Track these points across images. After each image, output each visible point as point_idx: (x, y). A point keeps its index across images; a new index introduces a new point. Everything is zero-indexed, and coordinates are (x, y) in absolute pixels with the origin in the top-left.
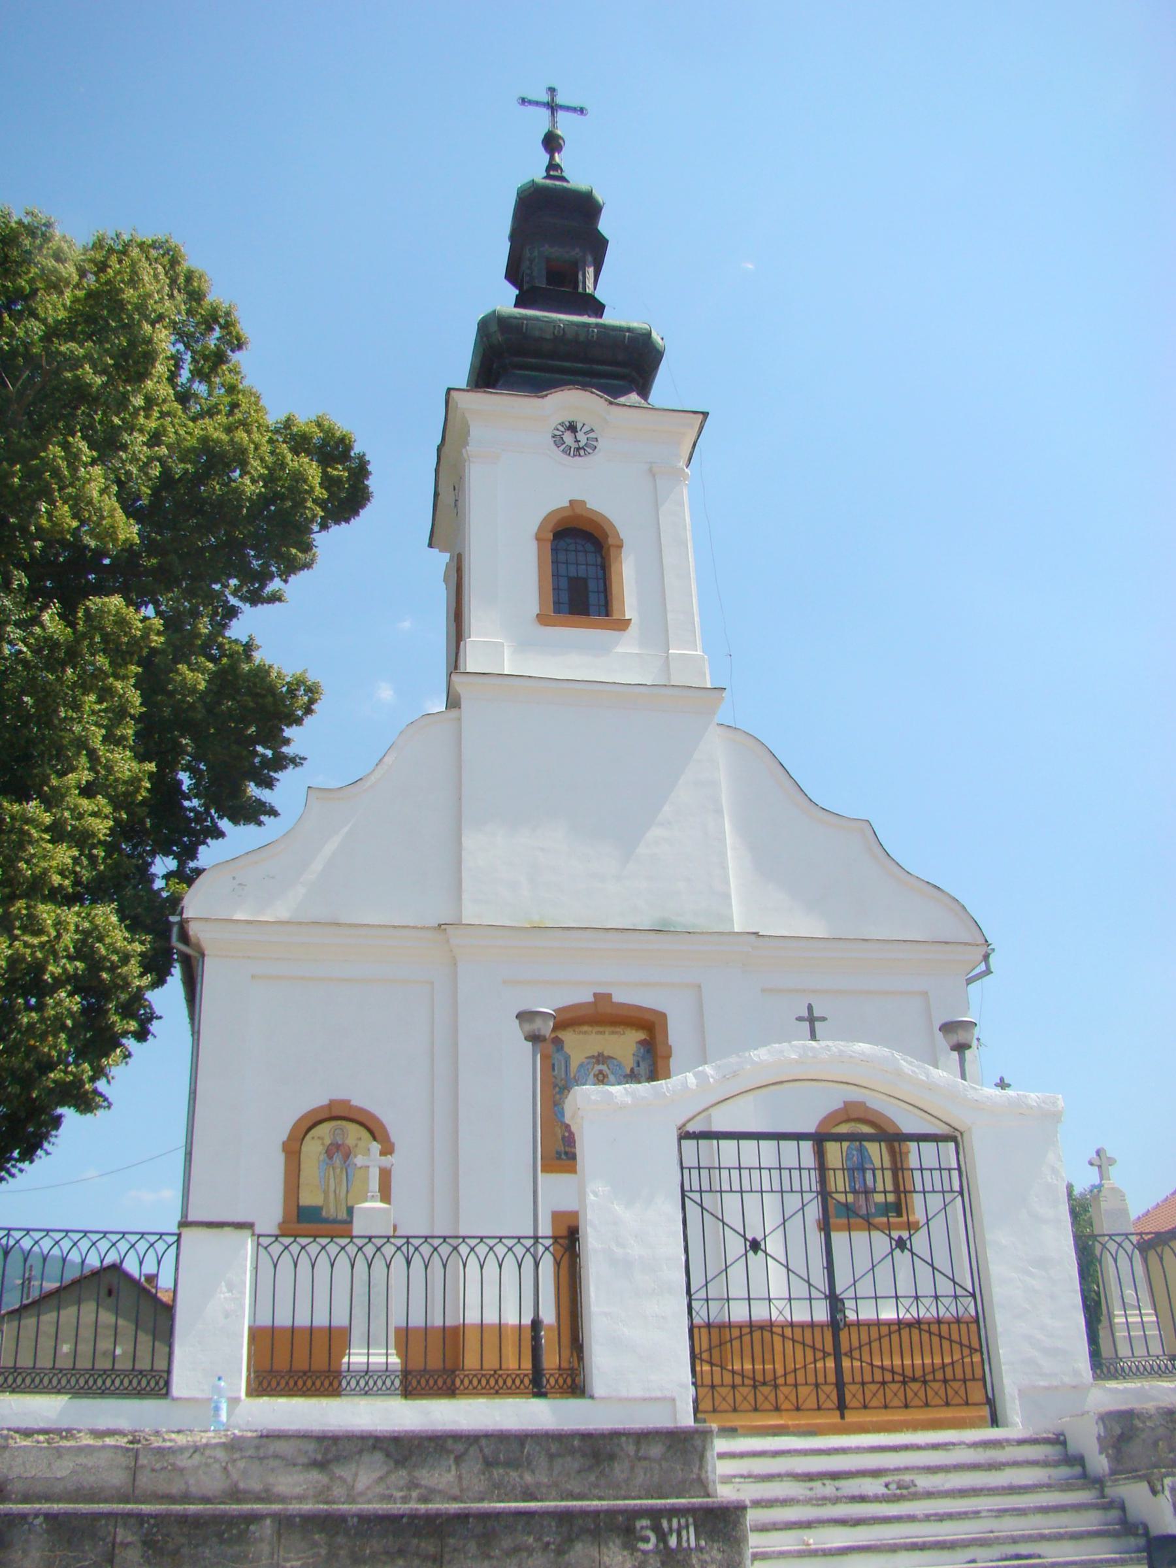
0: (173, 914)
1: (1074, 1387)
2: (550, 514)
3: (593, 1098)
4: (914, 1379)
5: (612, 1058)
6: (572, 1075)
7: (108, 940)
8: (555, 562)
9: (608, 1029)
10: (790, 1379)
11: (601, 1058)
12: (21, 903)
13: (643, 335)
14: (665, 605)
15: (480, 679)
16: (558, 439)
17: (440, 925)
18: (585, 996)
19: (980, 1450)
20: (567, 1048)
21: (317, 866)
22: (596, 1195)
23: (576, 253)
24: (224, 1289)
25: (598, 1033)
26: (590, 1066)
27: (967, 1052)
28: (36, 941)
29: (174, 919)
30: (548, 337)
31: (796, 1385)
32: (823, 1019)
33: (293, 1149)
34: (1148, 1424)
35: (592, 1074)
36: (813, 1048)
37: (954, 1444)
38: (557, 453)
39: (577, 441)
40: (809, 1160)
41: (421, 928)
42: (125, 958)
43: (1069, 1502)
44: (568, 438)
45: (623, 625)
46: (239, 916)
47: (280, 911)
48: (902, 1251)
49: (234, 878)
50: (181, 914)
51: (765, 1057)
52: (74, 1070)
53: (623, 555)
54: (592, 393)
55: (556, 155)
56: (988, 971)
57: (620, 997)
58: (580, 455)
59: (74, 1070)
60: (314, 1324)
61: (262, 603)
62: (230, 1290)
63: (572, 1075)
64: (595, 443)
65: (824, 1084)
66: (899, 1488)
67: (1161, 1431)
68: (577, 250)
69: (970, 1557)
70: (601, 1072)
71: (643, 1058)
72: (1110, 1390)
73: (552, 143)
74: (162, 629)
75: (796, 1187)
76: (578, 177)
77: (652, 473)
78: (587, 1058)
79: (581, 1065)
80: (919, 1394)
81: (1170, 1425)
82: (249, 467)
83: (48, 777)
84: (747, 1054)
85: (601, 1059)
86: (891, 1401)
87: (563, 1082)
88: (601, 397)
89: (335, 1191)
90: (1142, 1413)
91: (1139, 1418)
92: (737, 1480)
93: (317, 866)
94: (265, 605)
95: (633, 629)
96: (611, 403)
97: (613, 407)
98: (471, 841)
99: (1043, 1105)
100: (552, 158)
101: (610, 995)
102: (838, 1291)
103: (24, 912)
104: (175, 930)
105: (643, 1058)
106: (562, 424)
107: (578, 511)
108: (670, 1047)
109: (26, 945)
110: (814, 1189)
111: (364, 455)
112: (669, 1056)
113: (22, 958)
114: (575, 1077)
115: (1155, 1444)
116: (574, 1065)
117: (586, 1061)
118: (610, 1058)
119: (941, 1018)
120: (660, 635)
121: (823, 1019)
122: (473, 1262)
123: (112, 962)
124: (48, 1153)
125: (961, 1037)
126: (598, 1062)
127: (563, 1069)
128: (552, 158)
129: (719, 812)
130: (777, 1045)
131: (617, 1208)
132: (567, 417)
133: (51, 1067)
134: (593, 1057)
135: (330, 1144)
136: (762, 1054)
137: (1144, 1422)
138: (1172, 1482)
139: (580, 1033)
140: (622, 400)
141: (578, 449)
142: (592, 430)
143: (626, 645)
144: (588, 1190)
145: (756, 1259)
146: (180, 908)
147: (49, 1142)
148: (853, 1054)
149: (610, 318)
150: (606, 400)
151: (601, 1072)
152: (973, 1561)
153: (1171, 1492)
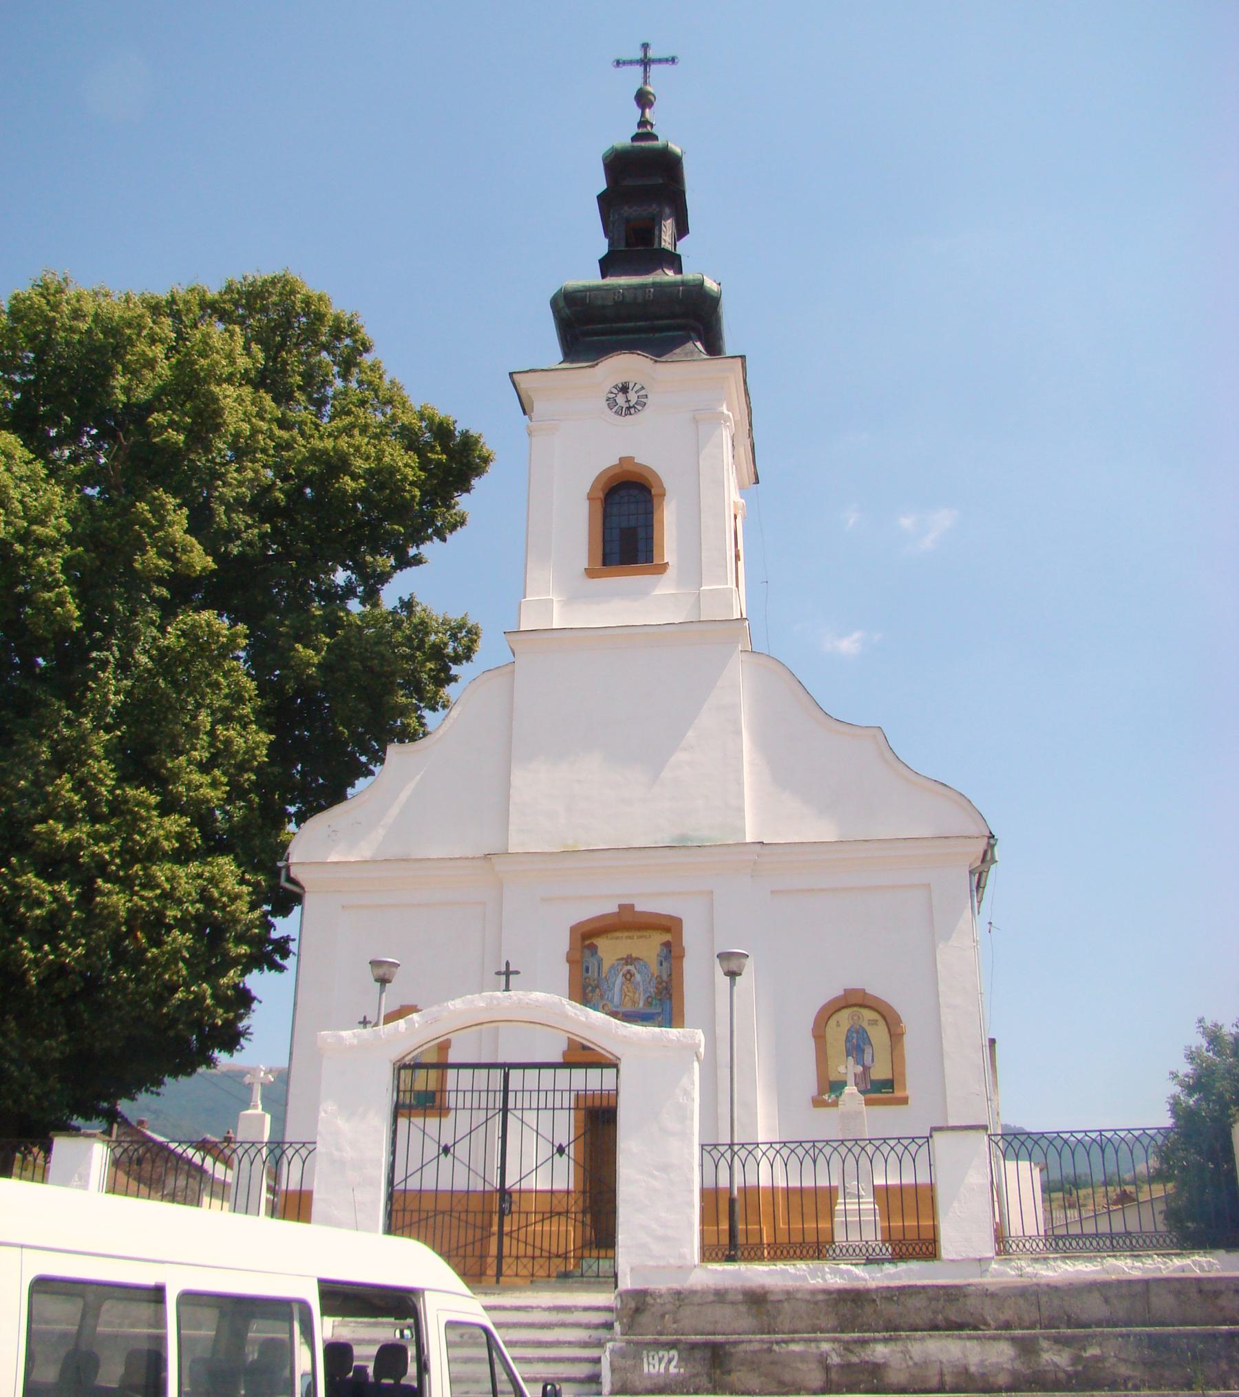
0: (281, 860)
1: (680, 1267)
2: (601, 474)
3: (329, 1040)
4: (558, 1256)
6: (604, 975)
7: (222, 885)
8: (606, 516)
9: (636, 934)
10: (461, 1251)
11: (629, 960)
12: (137, 867)
13: (695, 286)
15: (532, 636)
16: (611, 401)
18: (611, 907)
19: (554, 1313)
20: (600, 953)
21: (394, 811)
22: (326, 1112)
23: (654, 208)
24: (77, 1179)
25: (628, 937)
26: (619, 968)
27: (737, 978)
28: (150, 894)
29: (280, 864)
31: (465, 1257)
32: (517, 973)
34: (658, 1300)
36: (498, 998)
37: (532, 1308)
38: (611, 414)
39: (628, 401)
40: (497, 1083)
41: (472, 858)
42: (235, 898)
43: (586, 1356)
44: (621, 399)
45: (662, 568)
46: (333, 858)
47: (364, 851)
48: (561, 1156)
49: (329, 826)
50: (287, 860)
51: (459, 1006)
52: (196, 989)
53: (665, 503)
54: (639, 354)
55: (647, 110)
57: (639, 908)
58: (631, 414)
59: (196, 989)
60: (303, 1188)
61: (411, 567)
62: (80, 1180)
63: (604, 975)
65: (515, 1023)
66: (470, 1338)
67: (669, 1307)
68: (654, 206)
69: (466, 1390)
70: (629, 972)
72: (712, 1270)
73: (643, 100)
74: (248, 632)
75: (483, 1105)
77: (695, 421)
78: (618, 960)
79: (612, 967)
80: (528, 1266)
81: (677, 1303)
82: (353, 467)
83: (165, 762)
84: (445, 1004)
85: (629, 960)
86: (587, 1271)
87: (596, 982)
88: (647, 357)
89: (405, 1081)
90: (655, 1292)
91: (651, 1295)
92: (352, 1324)
93: (394, 811)
94: (414, 567)
95: (671, 572)
96: (656, 361)
97: (658, 364)
98: (519, 778)
99: (682, 1039)
100: (643, 114)
101: (632, 906)
102: (507, 1186)
103: (141, 873)
104: (283, 873)
106: (615, 387)
107: (627, 467)
108: (684, 949)
109: (143, 898)
110: (497, 1106)
111: (467, 431)
112: (682, 957)
113: (141, 909)
115: (663, 1316)
116: (606, 966)
117: (616, 963)
118: (637, 959)
119: (718, 951)
120: (694, 573)
121: (517, 973)
123: (224, 903)
124: (243, 1048)
125: (733, 966)
126: (627, 964)
127: (596, 970)
128: (643, 114)
129: (739, 733)
130: (470, 996)
131: (339, 1122)
132: (619, 381)
133: (174, 989)
134: (622, 959)
136: (457, 1004)
137: (655, 1299)
138: (613, 1346)
139: (612, 939)
140: (663, 359)
141: (629, 408)
142: (643, 388)
144: (321, 1109)
145: (446, 1161)
146: (286, 854)
147: (246, 1039)
148: (529, 1002)
150: (651, 359)
151: (629, 972)
152: (467, 1393)
153: (610, 1354)
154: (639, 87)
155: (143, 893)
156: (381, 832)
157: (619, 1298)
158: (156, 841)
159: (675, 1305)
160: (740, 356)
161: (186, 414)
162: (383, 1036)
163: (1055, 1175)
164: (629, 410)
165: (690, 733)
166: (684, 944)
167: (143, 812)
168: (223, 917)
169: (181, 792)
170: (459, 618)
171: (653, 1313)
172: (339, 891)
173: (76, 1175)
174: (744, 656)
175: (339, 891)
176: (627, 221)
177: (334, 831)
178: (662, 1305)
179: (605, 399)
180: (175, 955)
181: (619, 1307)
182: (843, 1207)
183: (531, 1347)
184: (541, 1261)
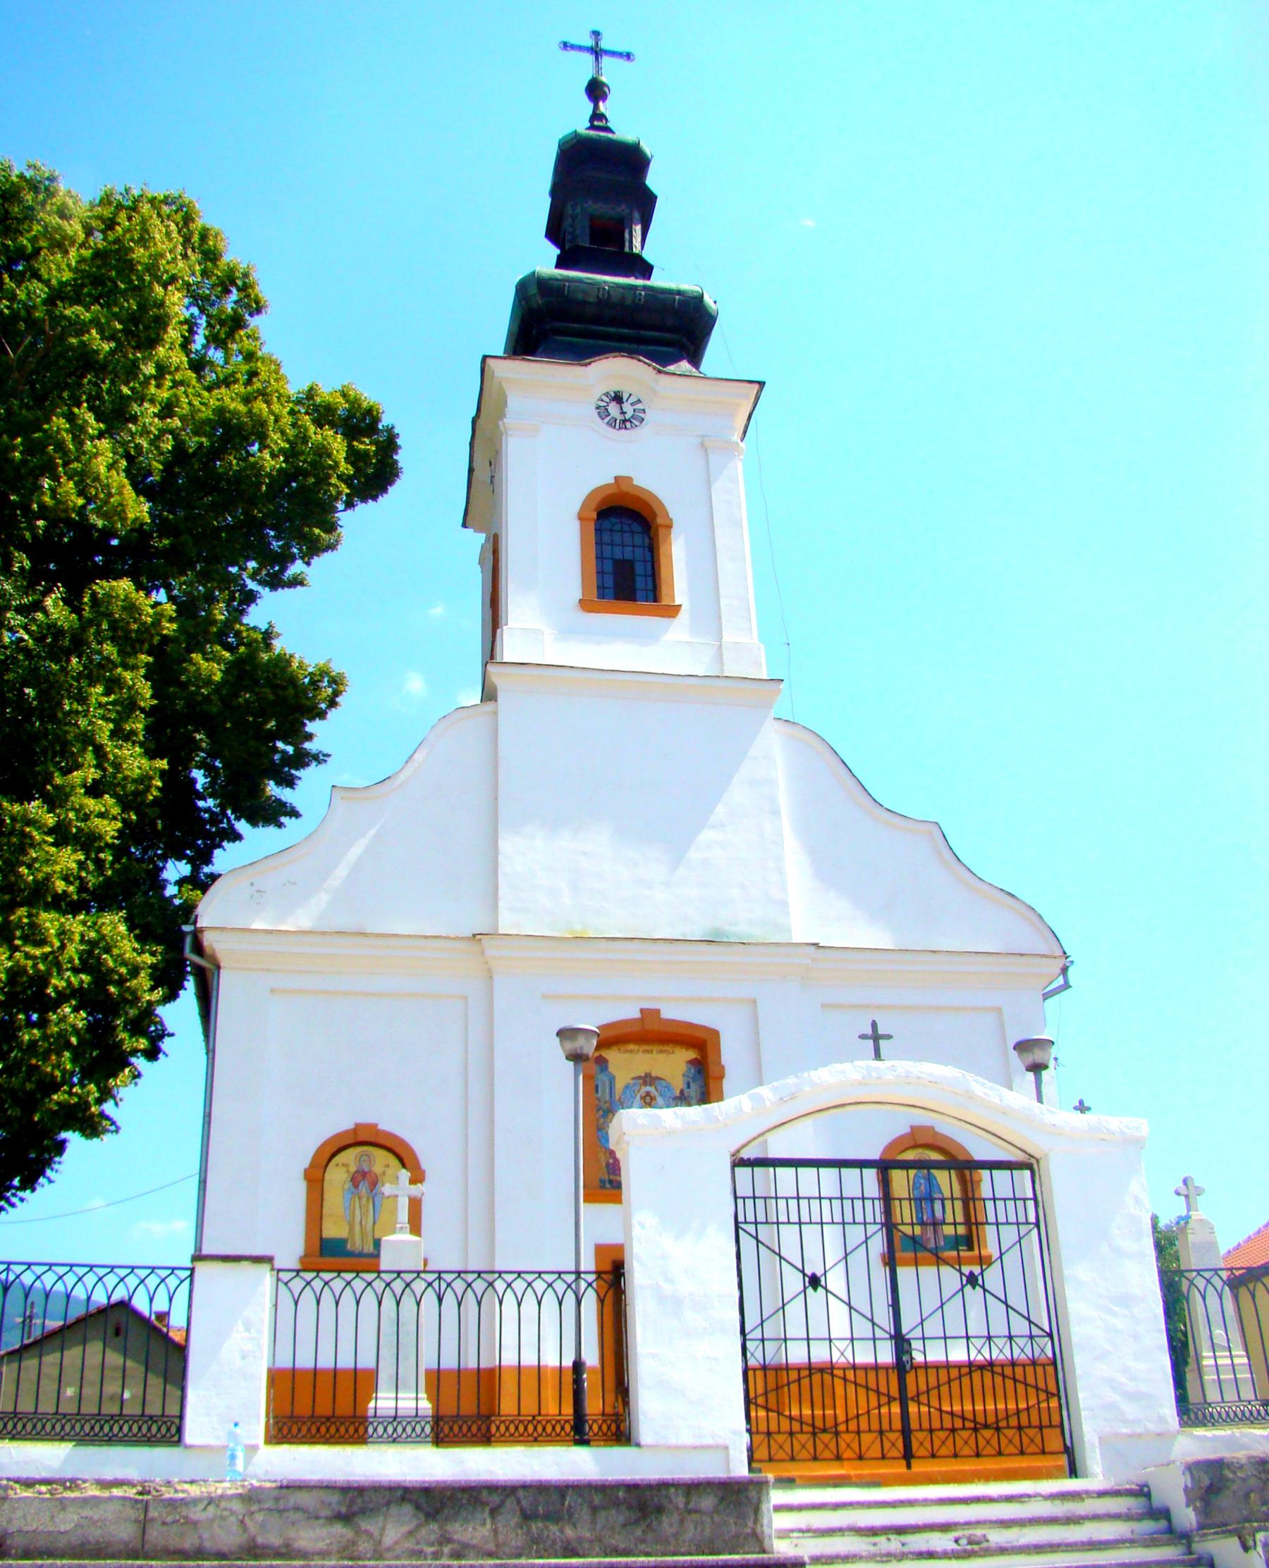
0: (186, 923)
1: (1159, 1435)
5: (660, 1079)
6: (617, 1097)
7: (116, 951)
8: (599, 543)
9: (656, 1048)
10: (853, 1425)
11: (648, 1079)
12: (22, 912)
13: (694, 298)
14: (717, 589)
15: (538, 671)
17: (474, 935)
19: (1058, 1502)
20: (612, 1068)
21: (342, 871)
23: (622, 210)
25: (645, 1051)
26: (636, 1088)
27: (1044, 1073)
29: (187, 928)
30: (592, 300)
31: (858, 1432)
32: (889, 1037)
33: (315, 1178)
34: (1239, 1474)
35: (638, 1097)
37: (1029, 1496)
38: (601, 425)
39: (623, 413)
40: (873, 1188)
42: (135, 971)
44: (614, 409)
45: (672, 611)
46: (258, 925)
47: (302, 919)
48: (974, 1288)
50: (195, 923)
52: (79, 1091)
54: (639, 360)
55: (601, 104)
56: (1066, 986)
58: (626, 428)
59: (79, 1091)
61: (283, 588)
62: (248, 1329)
63: (617, 1097)
64: (642, 415)
65: (889, 1107)
66: (970, 1543)
67: (1253, 1482)
68: (623, 206)
70: (648, 1094)
71: (694, 1079)
72: (1198, 1437)
73: (596, 91)
75: (859, 1218)
76: (624, 129)
77: (704, 447)
79: (627, 1087)
81: (1263, 1475)
85: (648, 1079)
86: (961, 1449)
91: (1229, 1468)
92: (795, 1534)
93: (342, 871)
95: (683, 615)
98: (508, 844)
100: (596, 107)
101: (658, 1011)
102: (904, 1331)
103: (26, 920)
105: (694, 1079)
106: (607, 394)
108: (723, 1067)
110: (878, 1220)
111: (393, 428)
112: (721, 1077)
114: (620, 1099)
115: (1247, 1496)
116: (619, 1085)
120: (713, 622)
121: (889, 1037)
122: (509, 1299)
123: (121, 975)
125: (1037, 1056)
126: (645, 1083)
128: (596, 107)
132: (613, 387)
134: (639, 1078)
135: (356, 1172)
137: (1234, 1473)
139: (626, 1051)
140: (672, 368)
141: (625, 421)
142: (639, 401)
143: (676, 630)
145: (816, 1296)
146: (193, 917)
148: (921, 1075)
149: (658, 280)
150: (654, 368)
151: (648, 1094)
153: (1263, 1548)
154: (590, 77)
155: (27, 949)
156: (325, 897)
157: (1187, 1474)
158: (48, 877)
159: (1260, 1479)
160: (759, 382)
161: (116, 316)
162: (721, 1118)
163: (449, 1408)
164: (625, 423)
165: (720, 809)
166: (723, 1062)
167: (37, 836)
168: (121, 995)
169: (71, 820)
170: (322, 662)
171: (1234, 1492)
172: (268, 970)
173: (240, 1322)
174: (777, 725)
175: (268, 970)
176: (592, 218)
177: (258, 891)
178: (1244, 1480)
179: (594, 407)
180: (62, 1042)
181: (1190, 1486)
182: (1212, 1362)
183: (1078, 1550)
184: (965, 1434)
